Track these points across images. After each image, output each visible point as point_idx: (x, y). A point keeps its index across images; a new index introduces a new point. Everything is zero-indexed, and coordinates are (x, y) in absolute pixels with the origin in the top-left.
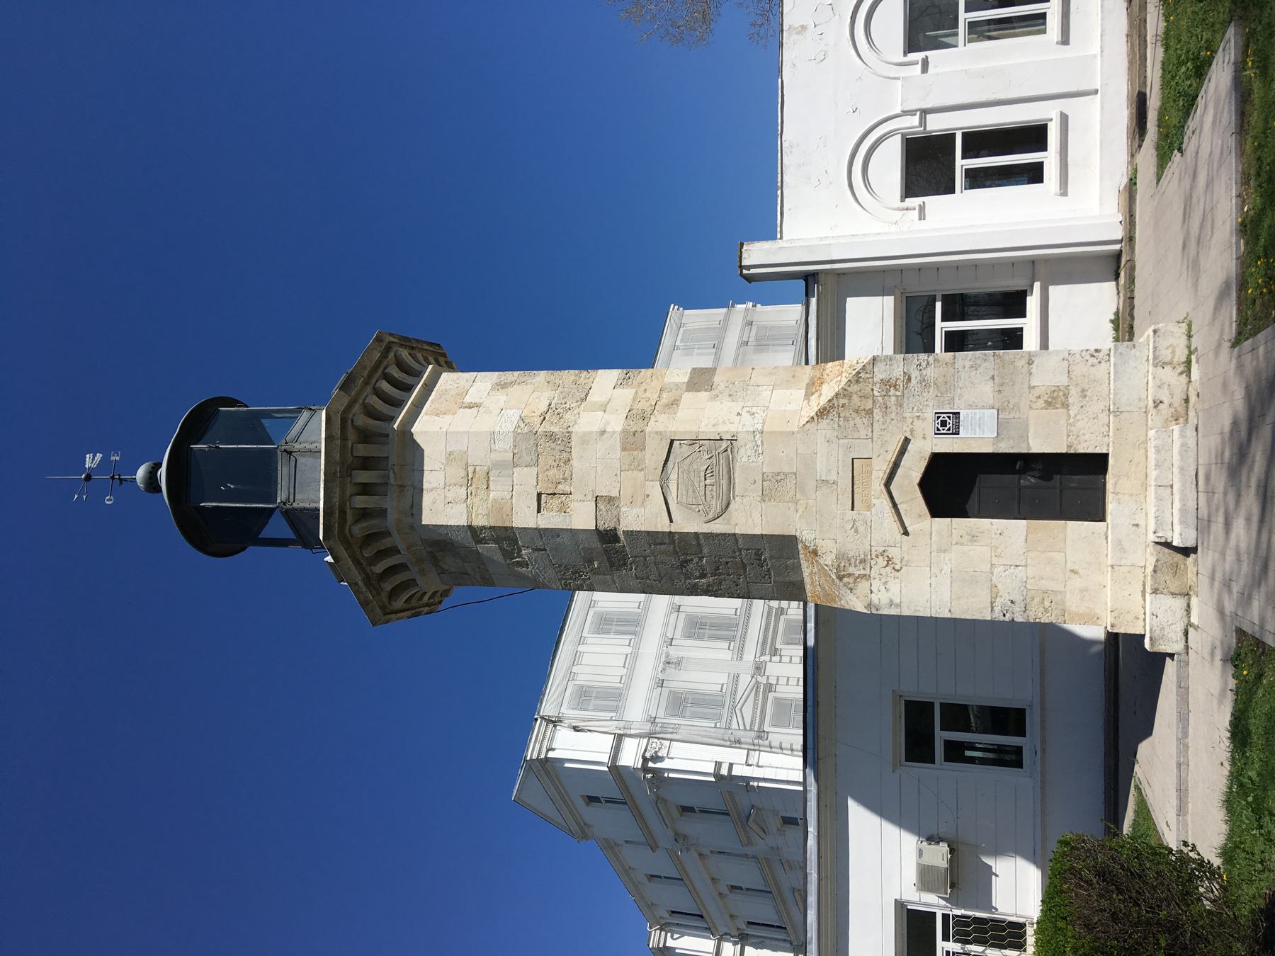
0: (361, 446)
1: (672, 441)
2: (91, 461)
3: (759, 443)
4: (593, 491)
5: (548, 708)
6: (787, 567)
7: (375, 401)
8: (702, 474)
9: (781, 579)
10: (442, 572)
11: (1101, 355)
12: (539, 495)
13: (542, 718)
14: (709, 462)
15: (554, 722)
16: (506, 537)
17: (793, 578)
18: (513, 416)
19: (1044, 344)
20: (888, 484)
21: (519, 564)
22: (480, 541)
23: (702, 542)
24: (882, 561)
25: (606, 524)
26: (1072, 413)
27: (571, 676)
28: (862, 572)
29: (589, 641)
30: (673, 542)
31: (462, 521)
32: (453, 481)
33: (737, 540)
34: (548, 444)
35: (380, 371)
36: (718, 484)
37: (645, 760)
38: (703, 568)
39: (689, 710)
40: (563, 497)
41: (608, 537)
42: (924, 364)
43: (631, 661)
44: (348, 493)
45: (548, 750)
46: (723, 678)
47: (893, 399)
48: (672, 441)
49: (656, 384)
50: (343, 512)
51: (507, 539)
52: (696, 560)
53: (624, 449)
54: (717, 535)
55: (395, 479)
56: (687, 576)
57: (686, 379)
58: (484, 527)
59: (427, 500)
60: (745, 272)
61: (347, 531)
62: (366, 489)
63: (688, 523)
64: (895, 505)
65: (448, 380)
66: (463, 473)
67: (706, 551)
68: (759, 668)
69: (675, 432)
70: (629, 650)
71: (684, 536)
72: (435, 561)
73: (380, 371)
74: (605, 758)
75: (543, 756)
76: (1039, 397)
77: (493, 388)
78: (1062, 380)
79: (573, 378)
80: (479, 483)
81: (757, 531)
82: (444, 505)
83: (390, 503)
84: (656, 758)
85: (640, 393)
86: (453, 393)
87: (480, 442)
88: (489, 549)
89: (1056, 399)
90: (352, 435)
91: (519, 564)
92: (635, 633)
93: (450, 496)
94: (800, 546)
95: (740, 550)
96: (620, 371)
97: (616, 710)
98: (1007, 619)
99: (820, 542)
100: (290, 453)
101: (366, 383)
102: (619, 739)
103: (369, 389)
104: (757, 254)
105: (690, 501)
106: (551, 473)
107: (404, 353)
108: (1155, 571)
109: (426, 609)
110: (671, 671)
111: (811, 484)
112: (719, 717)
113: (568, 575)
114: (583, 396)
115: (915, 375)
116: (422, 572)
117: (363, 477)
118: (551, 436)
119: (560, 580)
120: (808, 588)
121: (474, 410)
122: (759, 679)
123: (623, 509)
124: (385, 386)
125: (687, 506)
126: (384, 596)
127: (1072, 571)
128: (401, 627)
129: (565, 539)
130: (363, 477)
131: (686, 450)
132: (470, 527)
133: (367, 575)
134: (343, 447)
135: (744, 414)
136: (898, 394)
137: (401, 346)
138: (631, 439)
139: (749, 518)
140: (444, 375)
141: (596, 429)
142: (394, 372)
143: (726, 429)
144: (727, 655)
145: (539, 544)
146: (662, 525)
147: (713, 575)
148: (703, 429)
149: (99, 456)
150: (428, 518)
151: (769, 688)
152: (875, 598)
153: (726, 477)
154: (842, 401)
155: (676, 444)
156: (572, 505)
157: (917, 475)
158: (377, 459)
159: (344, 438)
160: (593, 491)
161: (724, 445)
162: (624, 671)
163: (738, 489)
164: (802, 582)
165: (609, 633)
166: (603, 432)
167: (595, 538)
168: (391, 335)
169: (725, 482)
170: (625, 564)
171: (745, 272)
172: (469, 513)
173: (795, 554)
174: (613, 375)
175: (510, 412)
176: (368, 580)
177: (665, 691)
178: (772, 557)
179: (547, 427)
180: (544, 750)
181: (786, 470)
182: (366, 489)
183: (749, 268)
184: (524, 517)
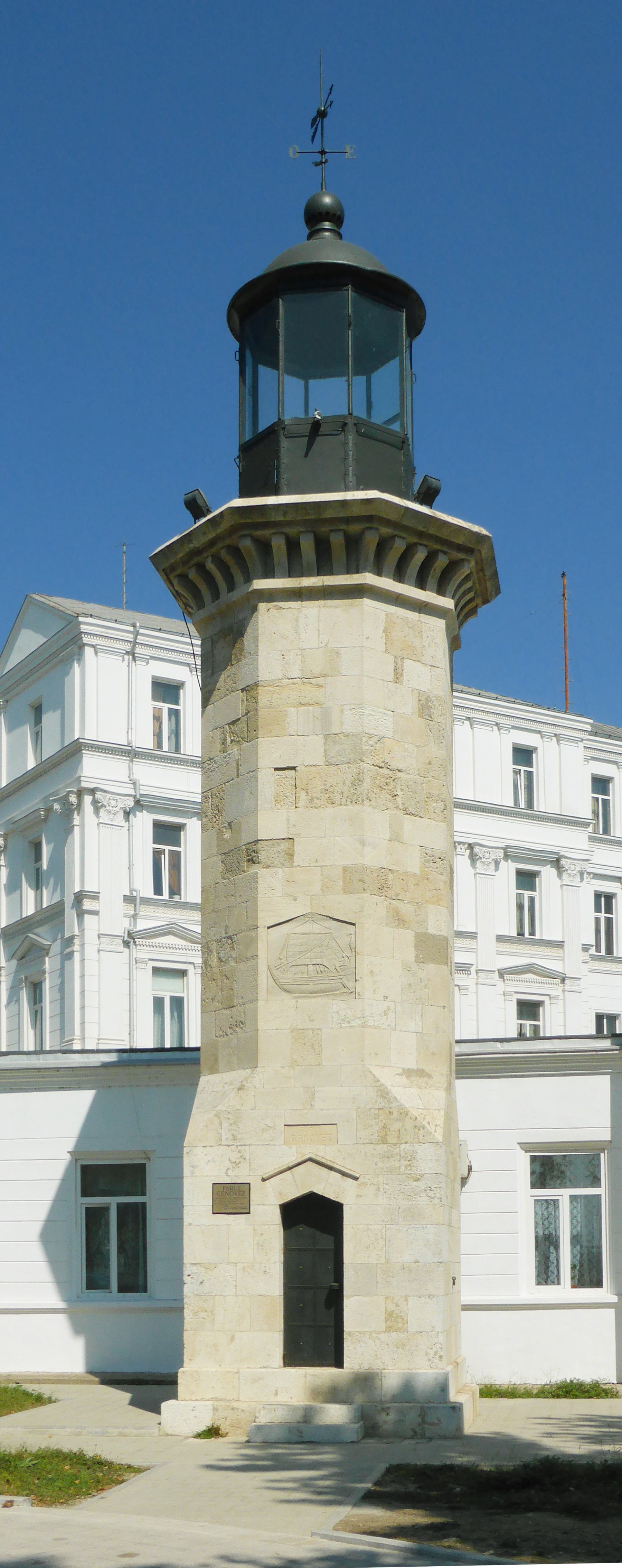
3: (353, 1023)
7: (400, 546)
11: (437, 1360)
14: (332, 968)
19: (466, 1308)
20: (310, 1160)
23: (250, 964)
24: (235, 1157)
26: (382, 1336)
28: (224, 1137)
35: (438, 547)
37: (93, 791)
42: (431, 1194)
47: (397, 1164)
50: (266, 525)
53: (345, 869)
54: (256, 980)
57: (432, 930)
61: (246, 532)
62: (293, 546)
63: (267, 945)
64: (290, 1168)
65: (438, 625)
73: (438, 547)
74: (91, 735)
75: (86, 639)
76: (397, 1305)
78: (412, 1327)
84: (97, 806)
89: (394, 1321)
90: (355, 528)
98: (186, 1279)
101: (421, 534)
103: (413, 539)
107: (465, 570)
108: (233, 1409)
114: (411, 810)
115: (421, 1185)
117: (307, 545)
118: (358, 780)
121: (391, 676)
123: (280, 871)
124: (420, 556)
127: (233, 1337)
130: (307, 545)
132: (257, 685)
136: (402, 1169)
137: (477, 563)
139: (275, 1016)
142: (442, 561)
146: (265, 918)
152: (199, 1151)
153: (317, 988)
154: (395, 1111)
157: (320, 1190)
159: (348, 520)
161: (350, 984)
163: (302, 1002)
166: (363, 843)
169: (311, 987)
172: (271, 684)
176: (198, 552)
182: (293, 546)
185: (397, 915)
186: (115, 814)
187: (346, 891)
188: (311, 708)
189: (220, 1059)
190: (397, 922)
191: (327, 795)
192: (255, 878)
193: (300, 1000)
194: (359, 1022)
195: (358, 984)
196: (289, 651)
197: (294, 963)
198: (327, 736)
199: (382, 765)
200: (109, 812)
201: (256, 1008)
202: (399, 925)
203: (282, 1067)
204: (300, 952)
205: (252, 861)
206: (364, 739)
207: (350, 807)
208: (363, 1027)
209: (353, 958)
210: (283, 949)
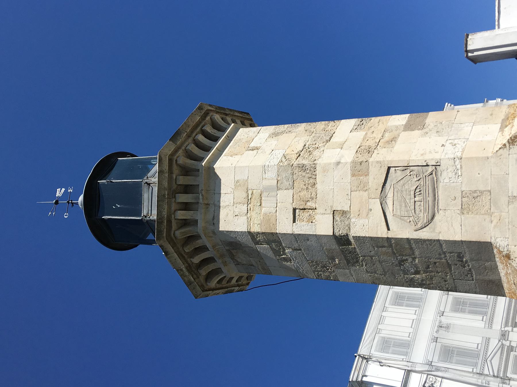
0: (181, 177)
1: (389, 168)
2: (59, 193)
3: (459, 167)
4: (332, 207)
5: (363, 350)
6: (485, 268)
8: (412, 193)
9: (481, 277)
10: (238, 264)
12: (294, 210)
13: (359, 355)
14: (418, 183)
15: (367, 359)
16: (273, 239)
17: (492, 277)
18: (279, 154)
21: (285, 260)
22: (257, 243)
25: (340, 231)
27: (378, 331)
29: (389, 309)
30: (391, 246)
31: (244, 229)
32: (239, 201)
33: (441, 245)
34: (302, 172)
36: (424, 200)
38: (416, 266)
39: (455, 358)
40: (311, 211)
41: (343, 241)
43: (416, 324)
44: (173, 209)
45: (363, 376)
46: (479, 340)
48: (389, 168)
49: (382, 128)
50: (169, 222)
51: (274, 241)
52: (410, 260)
53: (353, 175)
55: (203, 199)
56: (405, 272)
58: (258, 233)
59: (223, 214)
60: (470, 54)
62: (186, 207)
63: (401, 231)
65: (244, 133)
66: (245, 195)
67: (417, 253)
68: (504, 335)
69: (391, 161)
70: (415, 317)
71: (399, 241)
72: (232, 257)
75: (359, 380)
77: (270, 136)
79: (323, 126)
80: (255, 202)
81: (458, 238)
82: (232, 219)
83: (199, 216)
85: (369, 135)
86: (244, 141)
87: (264, 177)
88: (263, 248)
90: (176, 170)
91: (285, 260)
92: (419, 306)
93: (237, 211)
94: (495, 251)
95: (444, 253)
96: (356, 120)
97: (406, 354)
99: (512, 248)
100: (149, 184)
101: (189, 136)
102: (408, 373)
103: (190, 140)
104: (479, 41)
105: (403, 213)
106: (302, 194)
107: (217, 117)
109: (237, 288)
110: (442, 332)
111: (504, 200)
112: (476, 365)
113: (319, 268)
114: (328, 138)
116: (225, 264)
117: (183, 198)
118: (302, 167)
119: (314, 272)
120: (505, 285)
121: (255, 151)
122: (504, 342)
123: (353, 220)
124: (201, 138)
125: (401, 217)
126: (202, 279)
128: (218, 299)
129: (312, 242)
130: (183, 198)
131: (399, 174)
132: (249, 233)
133: (189, 265)
134: (170, 178)
135: (447, 145)
137: (217, 113)
138: (358, 167)
139: (450, 228)
140: (241, 130)
141: (334, 160)
143: (431, 158)
144: (481, 324)
145: (296, 246)
146: (382, 233)
147: (425, 272)
148: (414, 158)
149: (63, 189)
150: (223, 227)
151: (511, 349)
153: (431, 195)
155: (392, 170)
156: (317, 217)
158: (193, 187)
159: (171, 171)
160: (332, 207)
161: (430, 169)
162: (411, 330)
164: (500, 280)
165: (402, 306)
166: (338, 163)
167: (334, 241)
168: (210, 105)
169: (430, 199)
170: (357, 262)
171: (470, 54)
172: (249, 224)
173: (491, 257)
174: (352, 122)
175: (277, 152)
176: (189, 268)
177: (439, 345)
178: (472, 260)
179: (301, 161)
180: (360, 376)
181: (481, 188)
182: (186, 207)
183: (473, 51)
184: (285, 226)
185: (388, 142)
186: (436, 380)
187: (367, 175)
188: (263, 198)
189: (491, 278)
190: (393, 142)
191: (310, 188)
192: (357, 239)
193: (440, 207)
194: (458, 162)
195: (429, 164)
196: (234, 211)
197: (413, 211)
198: (278, 189)
199: (298, 155)
200: (435, 382)
201: (446, 241)
202: (395, 141)
203: (492, 222)
204: (406, 206)
205: (349, 243)
206: (281, 164)
207: (317, 172)
208: (461, 159)
209: (412, 168)
210: (403, 220)
